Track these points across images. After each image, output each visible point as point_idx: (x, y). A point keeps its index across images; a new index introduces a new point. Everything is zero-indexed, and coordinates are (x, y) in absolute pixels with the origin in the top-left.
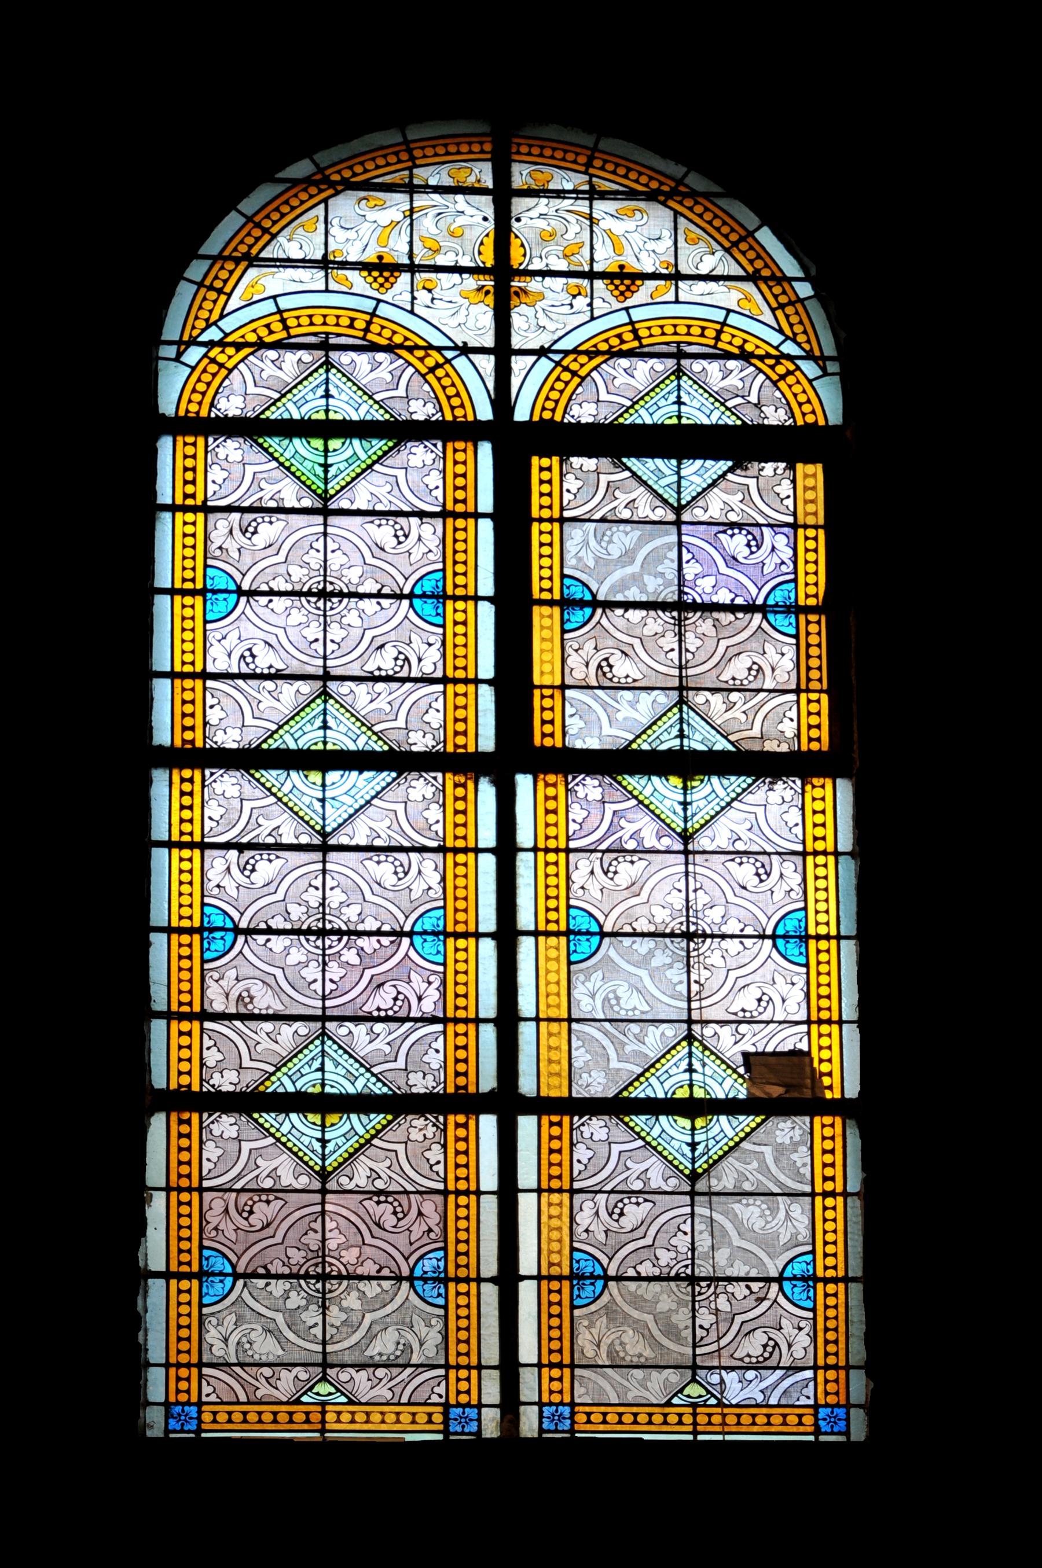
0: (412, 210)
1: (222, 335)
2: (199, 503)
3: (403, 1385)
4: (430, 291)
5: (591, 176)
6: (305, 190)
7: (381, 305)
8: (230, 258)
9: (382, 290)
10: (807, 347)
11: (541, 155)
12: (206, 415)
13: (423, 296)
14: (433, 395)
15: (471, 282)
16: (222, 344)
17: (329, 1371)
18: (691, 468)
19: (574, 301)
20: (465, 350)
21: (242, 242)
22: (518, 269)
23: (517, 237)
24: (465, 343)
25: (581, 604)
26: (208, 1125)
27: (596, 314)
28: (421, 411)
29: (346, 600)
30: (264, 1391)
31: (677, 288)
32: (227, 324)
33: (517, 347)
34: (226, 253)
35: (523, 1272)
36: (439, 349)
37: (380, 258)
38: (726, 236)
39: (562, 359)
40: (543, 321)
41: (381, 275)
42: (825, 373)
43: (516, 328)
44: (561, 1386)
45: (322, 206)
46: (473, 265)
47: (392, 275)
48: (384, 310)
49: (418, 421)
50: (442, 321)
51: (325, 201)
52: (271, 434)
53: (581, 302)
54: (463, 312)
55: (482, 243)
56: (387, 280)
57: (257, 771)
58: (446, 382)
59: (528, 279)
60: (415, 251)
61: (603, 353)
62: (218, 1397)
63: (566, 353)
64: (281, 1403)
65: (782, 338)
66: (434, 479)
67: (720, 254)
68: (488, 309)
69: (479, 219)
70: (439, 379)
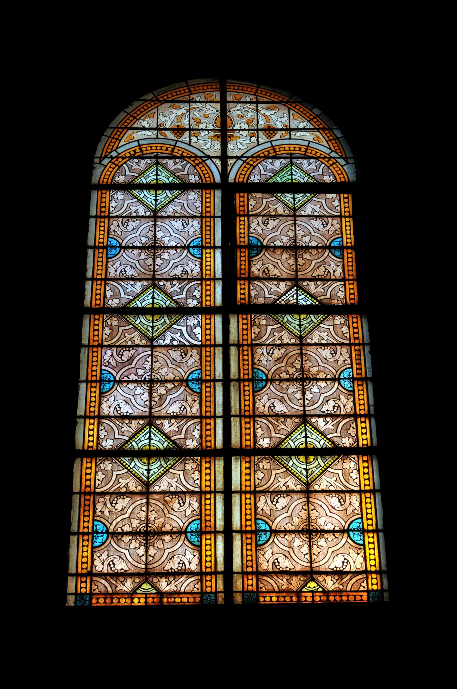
0: (190, 109)
1: (117, 154)
2: (106, 215)
3: (181, 584)
4: (196, 137)
5: (257, 96)
6: (150, 103)
7: (178, 143)
8: (120, 128)
9: (178, 137)
10: (340, 154)
11: (238, 89)
12: (233, 181)
13: (194, 139)
15: (212, 134)
16: (117, 157)
18: (299, 196)
21: (125, 122)
25: (335, 248)
26: (99, 464)
27: (260, 143)
28: (193, 179)
32: (120, 150)
33: (229, 156)
36: (200, 157)
37: (178, 126)
38: (308, 117)
39: (247, 160)
40: (239, 146)
41: (269, 133)
42: (347, 163)
43: (229, 148)
44: (251, 582)
45: (156, 109)
47: (274, 132)
48: (179, 144)
49: (327, 183)
50: (201, 147)
51: (157, 107)
53: (254, 139)
54: (209, 144)
55: (216, 120)
56: (272, 134)
57: (126, 315)
59: (234, 131)
60: (191, 123)
63: (248, 158)
65: (330, 151)
66: (198, 204)
67: (306, 123)
68: (218, 142)
69: (215, 111)
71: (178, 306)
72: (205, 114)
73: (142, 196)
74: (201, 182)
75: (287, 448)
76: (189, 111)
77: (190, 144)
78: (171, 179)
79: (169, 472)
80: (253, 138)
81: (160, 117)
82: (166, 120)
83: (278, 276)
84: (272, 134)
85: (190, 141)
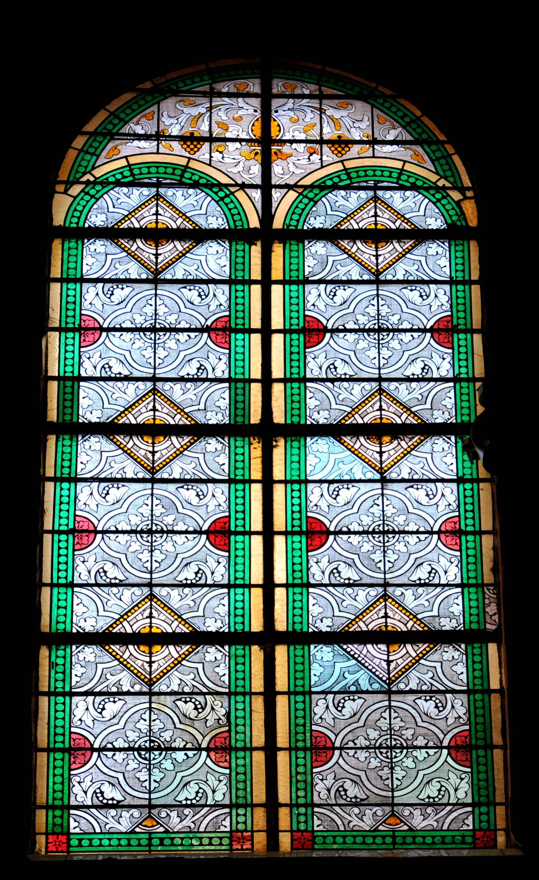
4: (221, 152)
9: (192, 152)
13: (217, 156)
14: (222, 212)
15: (246, 148)
16: (95, 183)
17: (152, 811)
19: (311, 157)
20: (243, 186)
22: (275, 139)
23: (275, 120)
24: (243, 183)
27: (324, 165)
29: (168, 334)
30: (112, 824)
31: (374, 149)
32: (98, 173)
34: (99, 130)
35: (279, 745)
36: (227, 186)
40: (292, 168)
41: (192, 144)
46: (248, 137)
47: (199, 144)
48: (192, 164)
50: (229, 170)
51: (158, 103)
52: (343, 239)
53: (315, 158)
55: (253, 125)
56: (343, 149)
58: (231, 206)
61: (112, 183)
62: (81, 830)
63: (305, 187)
64: (122, 833)
65: (438, 177)
67: (400, 129)
68: (256, 162)
70: (226, 204)
71: (419, 421)
72: (236, 116)
73: (354, 250)
74: (227, 228)
75: (120, 632)
76: (210, 109)
77: (210, 165)
78: (398, 223)
79: (420, 663)
80: (315, 155)
81: (163, 119)
82: (172, 124)
83: (350, 376)
84: (343, 149)
85: (210, 160)
